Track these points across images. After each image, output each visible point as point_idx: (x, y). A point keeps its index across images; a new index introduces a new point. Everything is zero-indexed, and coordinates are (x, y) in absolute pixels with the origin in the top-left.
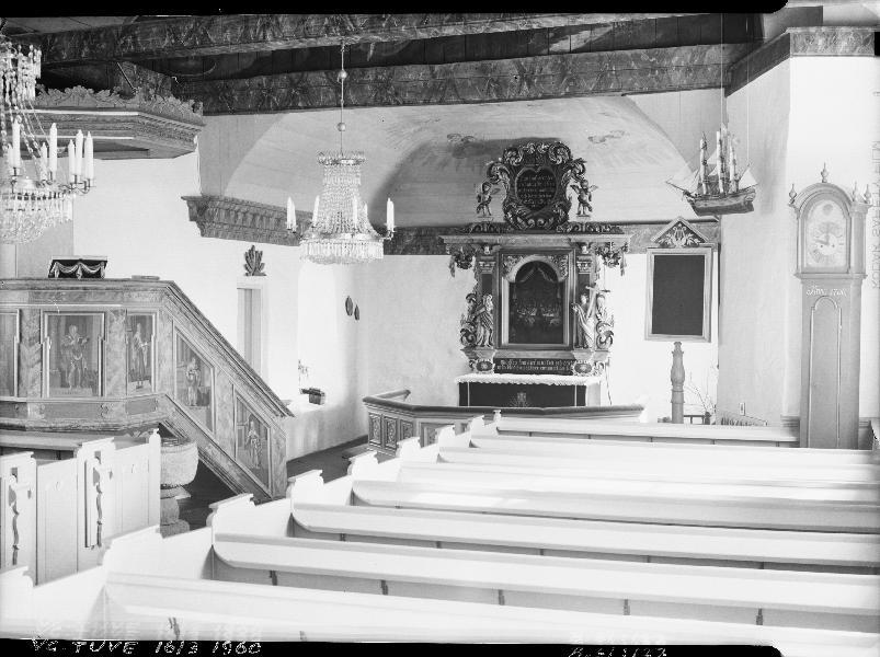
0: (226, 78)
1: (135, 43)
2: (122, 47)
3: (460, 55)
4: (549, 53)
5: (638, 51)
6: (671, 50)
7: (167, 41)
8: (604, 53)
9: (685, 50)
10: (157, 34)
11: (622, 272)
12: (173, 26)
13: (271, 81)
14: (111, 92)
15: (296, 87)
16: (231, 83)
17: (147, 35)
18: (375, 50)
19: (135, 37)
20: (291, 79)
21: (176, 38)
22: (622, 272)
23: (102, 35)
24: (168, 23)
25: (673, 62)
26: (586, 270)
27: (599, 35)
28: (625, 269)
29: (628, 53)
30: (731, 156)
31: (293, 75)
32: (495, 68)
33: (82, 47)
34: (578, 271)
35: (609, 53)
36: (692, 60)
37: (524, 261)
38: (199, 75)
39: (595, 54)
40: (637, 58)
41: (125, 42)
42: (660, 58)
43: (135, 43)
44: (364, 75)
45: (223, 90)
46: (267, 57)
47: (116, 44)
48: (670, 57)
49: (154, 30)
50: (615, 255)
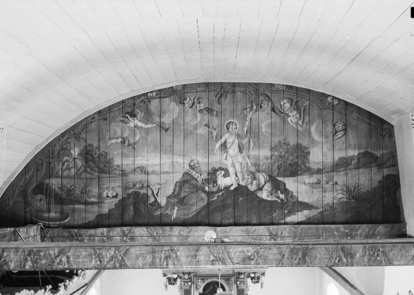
0: (79, 227)
1: (68, 262)
2: (59, 264)
3: (231, 221)
4: (285, 224)
5: (339, 226)
6: (357, 226)
7: (93, 263)
8: (318, 226)
9: (364, 226)
10: (85, 257)
11: (262, 287)
12: (98, 251)
13: (109, 231)
14: (45, 290)
15: (126, 236)
16: (83, 231)
17: (78, 257)
18: (177, 213)
19: (68, 258)
20: (124, 232)
21: (101, 261)
22: (262, 287)
23: (42, 254)
24: (94, 249)
25: (358, 233)
26: (242, 286)
27: (314, 214)
28: (263, 285)
29: (333, 226)
30: (80, 94)
31: (125, 228)
32: (254, 231)
33: (26, 260)
34: (238, 287)
35: (322, 226)
36: (369, 232)
37: (209, 281)
38: (58, 223)
39: (313, 226)
40: (338, 230)
41: (61, 261)
42: (352, 230)
43: (68, 262)
44: (172, 231)
45: (76, 236)
46: (106, 214)
47: (53, 262)
48: (357, 230)
49: (83, 253)
50: (258, 278)
